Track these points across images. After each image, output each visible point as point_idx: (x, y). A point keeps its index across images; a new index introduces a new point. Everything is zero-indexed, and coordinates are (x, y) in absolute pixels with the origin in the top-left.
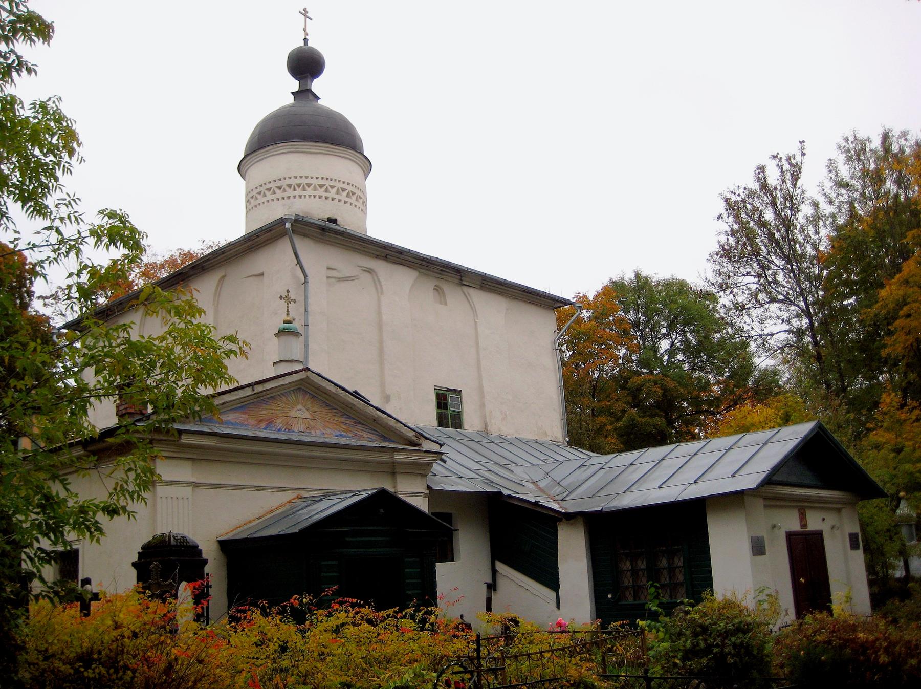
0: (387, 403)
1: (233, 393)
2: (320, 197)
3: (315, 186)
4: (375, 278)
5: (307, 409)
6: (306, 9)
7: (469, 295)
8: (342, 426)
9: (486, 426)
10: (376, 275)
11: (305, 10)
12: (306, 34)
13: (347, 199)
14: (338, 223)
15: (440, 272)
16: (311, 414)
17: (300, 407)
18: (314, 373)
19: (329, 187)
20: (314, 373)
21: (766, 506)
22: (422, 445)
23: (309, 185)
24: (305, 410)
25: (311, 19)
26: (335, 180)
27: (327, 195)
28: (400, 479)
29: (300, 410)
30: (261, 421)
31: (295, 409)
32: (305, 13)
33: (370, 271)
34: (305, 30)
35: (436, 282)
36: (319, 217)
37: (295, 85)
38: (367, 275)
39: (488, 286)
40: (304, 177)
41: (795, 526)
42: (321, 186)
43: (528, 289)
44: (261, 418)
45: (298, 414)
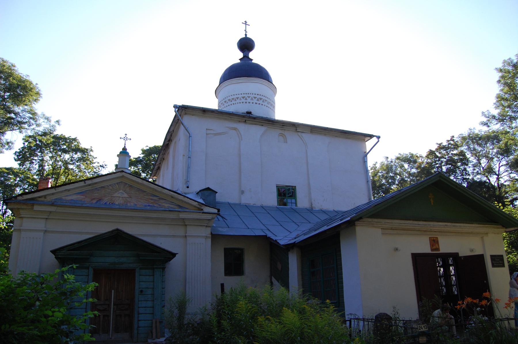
0: (242, 194)
1: (70, 185)
2: (243, 103)
3: (240, 98)
4: (238, 132)
5: (125, 192)
6: (246, 21)
7: (302, 137)
8: (150, 200)
9: (312, 204)
10: (238, 130)
11: (246, 22)
12: (246, 32)
13: (263, 103)
14: (252, 114)
15: (282, 126)
16: (128, 195)
17: (121, 191)
18: (127, 173)
19: (247, 97)
20: (127, 173)
21: (383, 234)
22: (204, 210)
23: (238, 98)
24: (124, 193)
25: (242, 23)
26: (262, 95)
27: (253, 101)
28: (189, 228)
29: (121, 193)
30: (94, 199)
31: (118, 193)
32: (246, 23)
33: (235, 129)
34: (245, 31)
35: (281, 132)
36: (242, 112)
37: (241, 55)
38: (234, 131)
39: (315, 131)
40: (238, 94)
41: (425, 248)
42: (243, 97)
43: (188, 106)
44: (93, 198)
45: (119, 195)
